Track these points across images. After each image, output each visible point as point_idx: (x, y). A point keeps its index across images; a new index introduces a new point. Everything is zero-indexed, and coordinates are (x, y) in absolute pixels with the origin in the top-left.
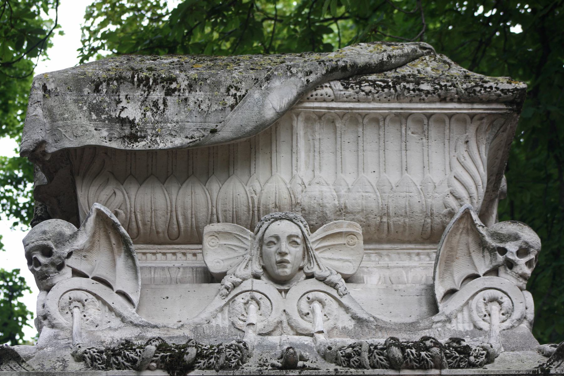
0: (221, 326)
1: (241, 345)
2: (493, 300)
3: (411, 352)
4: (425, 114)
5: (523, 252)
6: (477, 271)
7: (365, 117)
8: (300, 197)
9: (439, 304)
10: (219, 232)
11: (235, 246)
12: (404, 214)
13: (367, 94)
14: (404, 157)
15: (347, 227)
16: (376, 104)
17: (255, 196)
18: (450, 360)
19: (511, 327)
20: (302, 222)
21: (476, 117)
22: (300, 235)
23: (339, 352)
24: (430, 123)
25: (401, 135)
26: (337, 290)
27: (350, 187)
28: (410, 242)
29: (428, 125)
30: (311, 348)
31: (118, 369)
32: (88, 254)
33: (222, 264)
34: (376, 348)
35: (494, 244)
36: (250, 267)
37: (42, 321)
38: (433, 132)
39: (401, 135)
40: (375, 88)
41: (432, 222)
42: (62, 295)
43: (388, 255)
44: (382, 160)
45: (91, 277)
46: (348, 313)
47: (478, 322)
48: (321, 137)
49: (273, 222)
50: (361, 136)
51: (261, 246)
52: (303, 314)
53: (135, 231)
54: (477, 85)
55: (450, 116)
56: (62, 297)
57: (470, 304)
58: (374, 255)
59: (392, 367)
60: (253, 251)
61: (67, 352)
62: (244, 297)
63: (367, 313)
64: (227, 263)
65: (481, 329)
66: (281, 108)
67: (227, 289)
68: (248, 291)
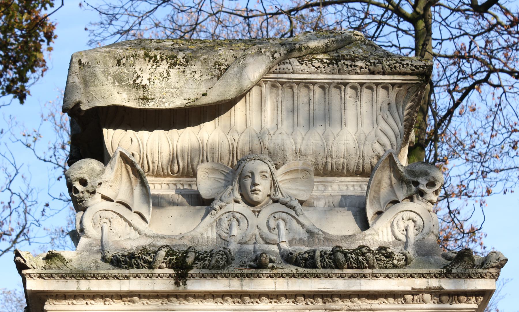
0: (211, 237)
26: (296, 211)
45: (115, 201)
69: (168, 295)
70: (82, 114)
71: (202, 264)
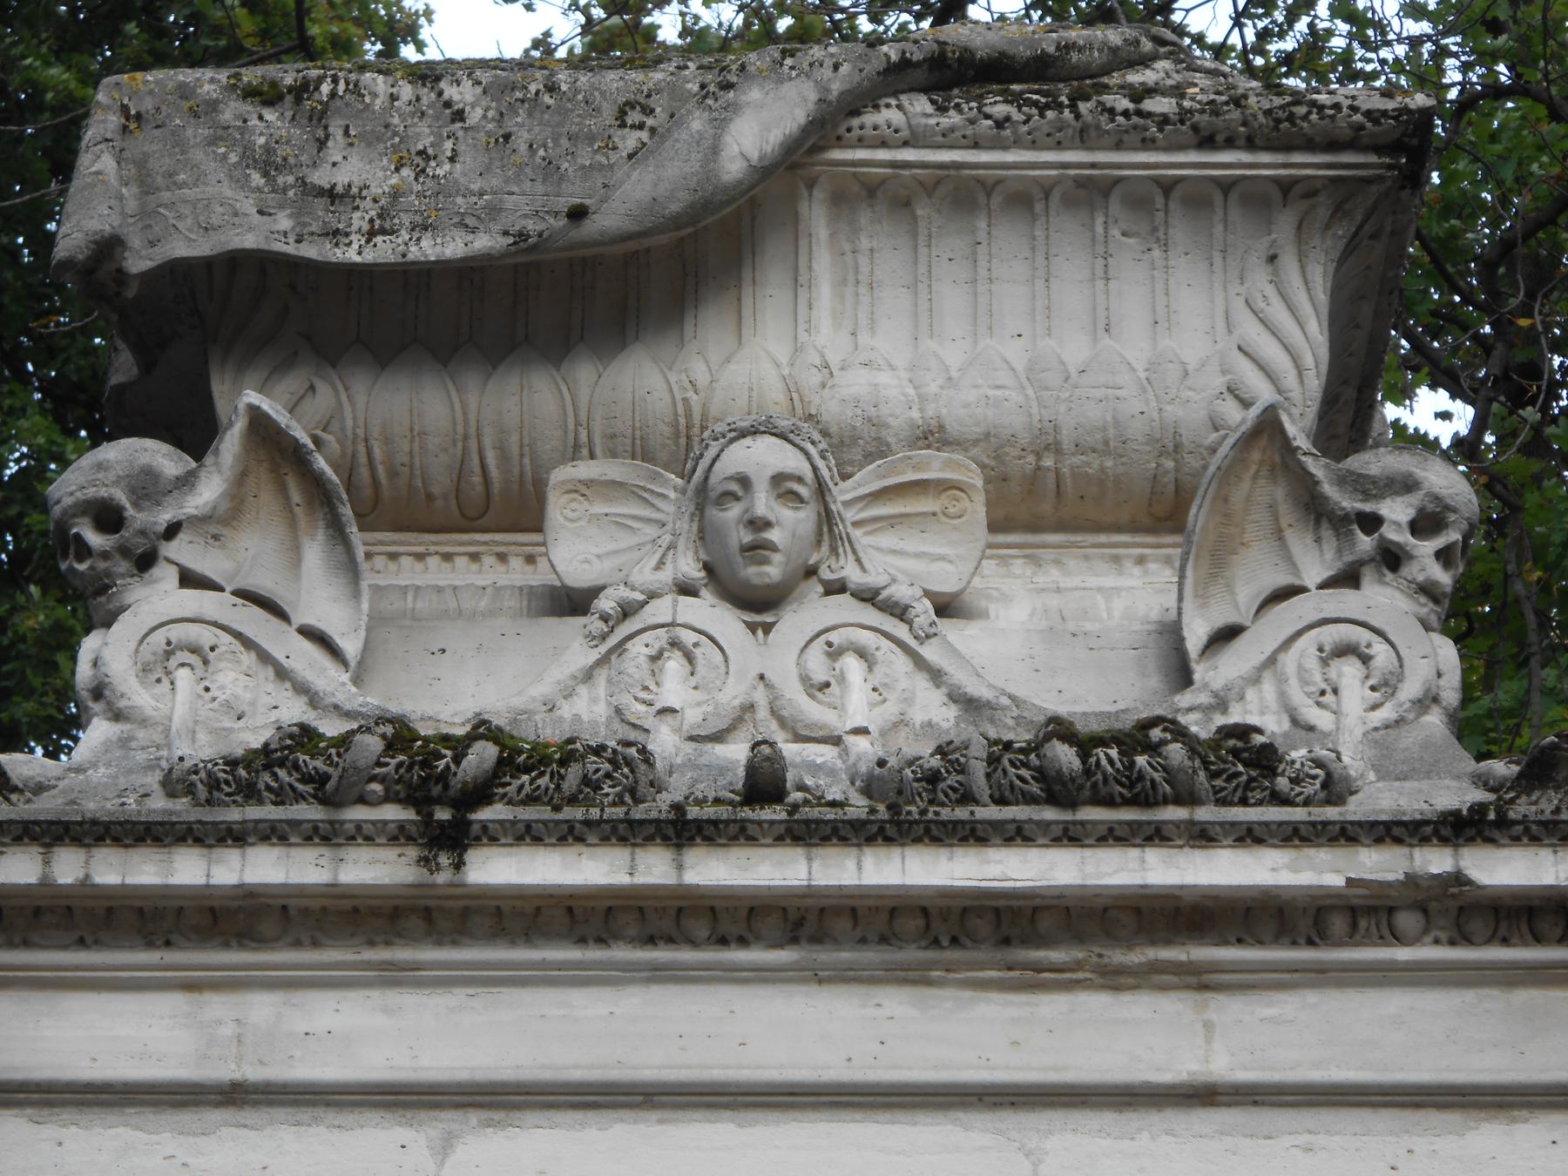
0: (585, 718)
1: (633, 751)
2: (1345, 650)
3: (1107, 755)
4: (1156, 180)
5: (1424, 525)
6: (1300, 578)
7: (993, 189)
8: (816, 400)
9: (1194, 665)
10: (589, 483)
11: (634, 517)
12: (1100, 447)
13: (1000, 124)
14: (1101, 298)
15: (942, 470)
16: (1024, 152)
17: (695, 397)
18: (1218, 783)
19: (1397, 722)
20: (813, 443)
21: (1297, 190)
22: (808, 475)
23: (908, 771)
24: (1172, 205)
25: (1093, 239)
26: (910, 623)
27: (954, 374)
28: (1117, 528)
29: (1166, 212)
30: (832, 773)
31: (275, 804)
32: (225, 531)
33: (597, 565)
34: (1008, 746)
35: (1348, 503)
36: (669, 566)
37: (91, 704)
38: (1179, 232)
39: (1093, 239)
40: (1019, 108)
41: (1177, 470)
42: (147, 635)
43: (1057, 562)
44: (1039, 304)
45: (229, 589)
46: (938, 687)
47: (1304, 710)
48: (875, 244)
49: (732, 441)
50: (985, 242)
51: (700, 509)
52: (812, 686)
53: (368, 492)
54: (1297, 103)
55: (1226, 187)
56: (148, 640)
57: (1279, 665)
58: (1020, 561)
59: (1052, 799)
60: (678, 524)
61: (149, 779)
62: (650, 641)
63: (990, 686)
64: (609, 564)
65: (1311, 728)
66: (761, 158)
67: (605, 618)
68: (663, 626)
69: (396, 908)
70: (131, 292)
71: (527, 789)
